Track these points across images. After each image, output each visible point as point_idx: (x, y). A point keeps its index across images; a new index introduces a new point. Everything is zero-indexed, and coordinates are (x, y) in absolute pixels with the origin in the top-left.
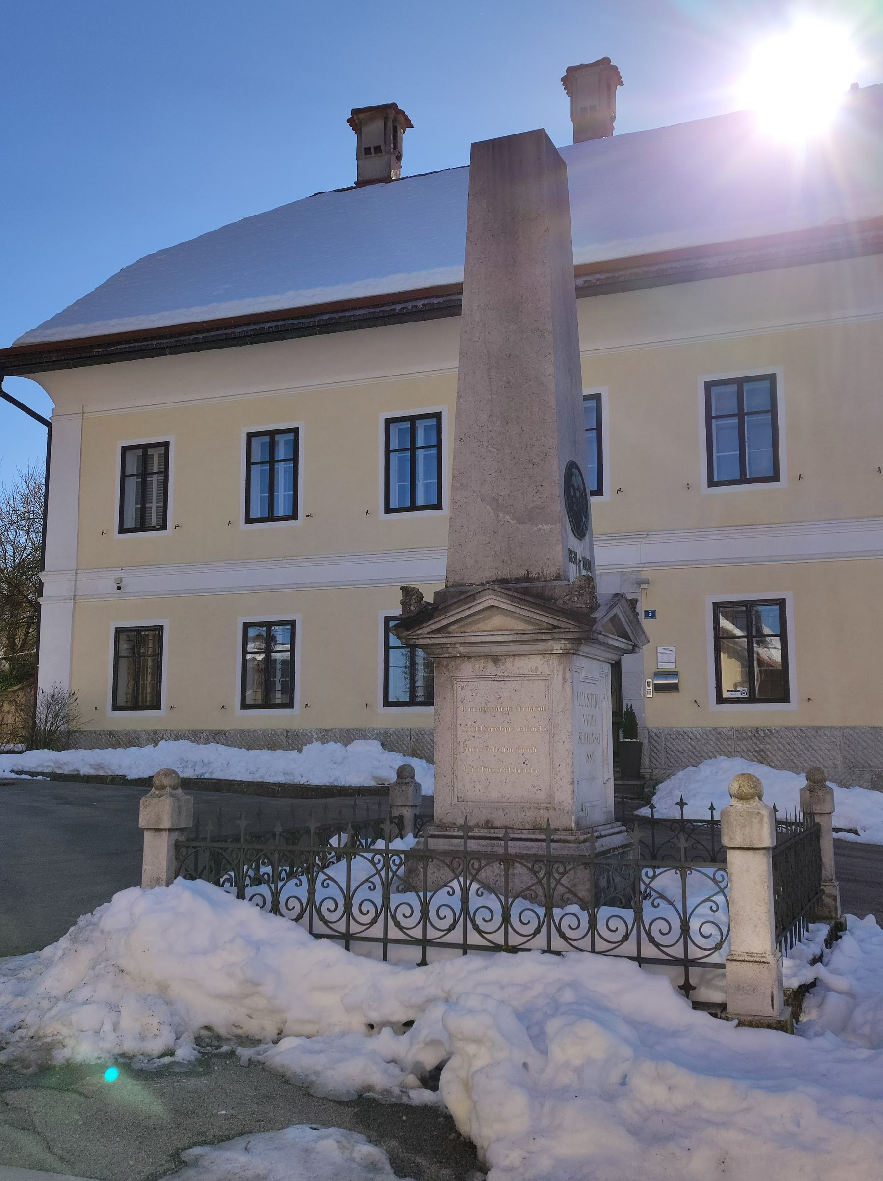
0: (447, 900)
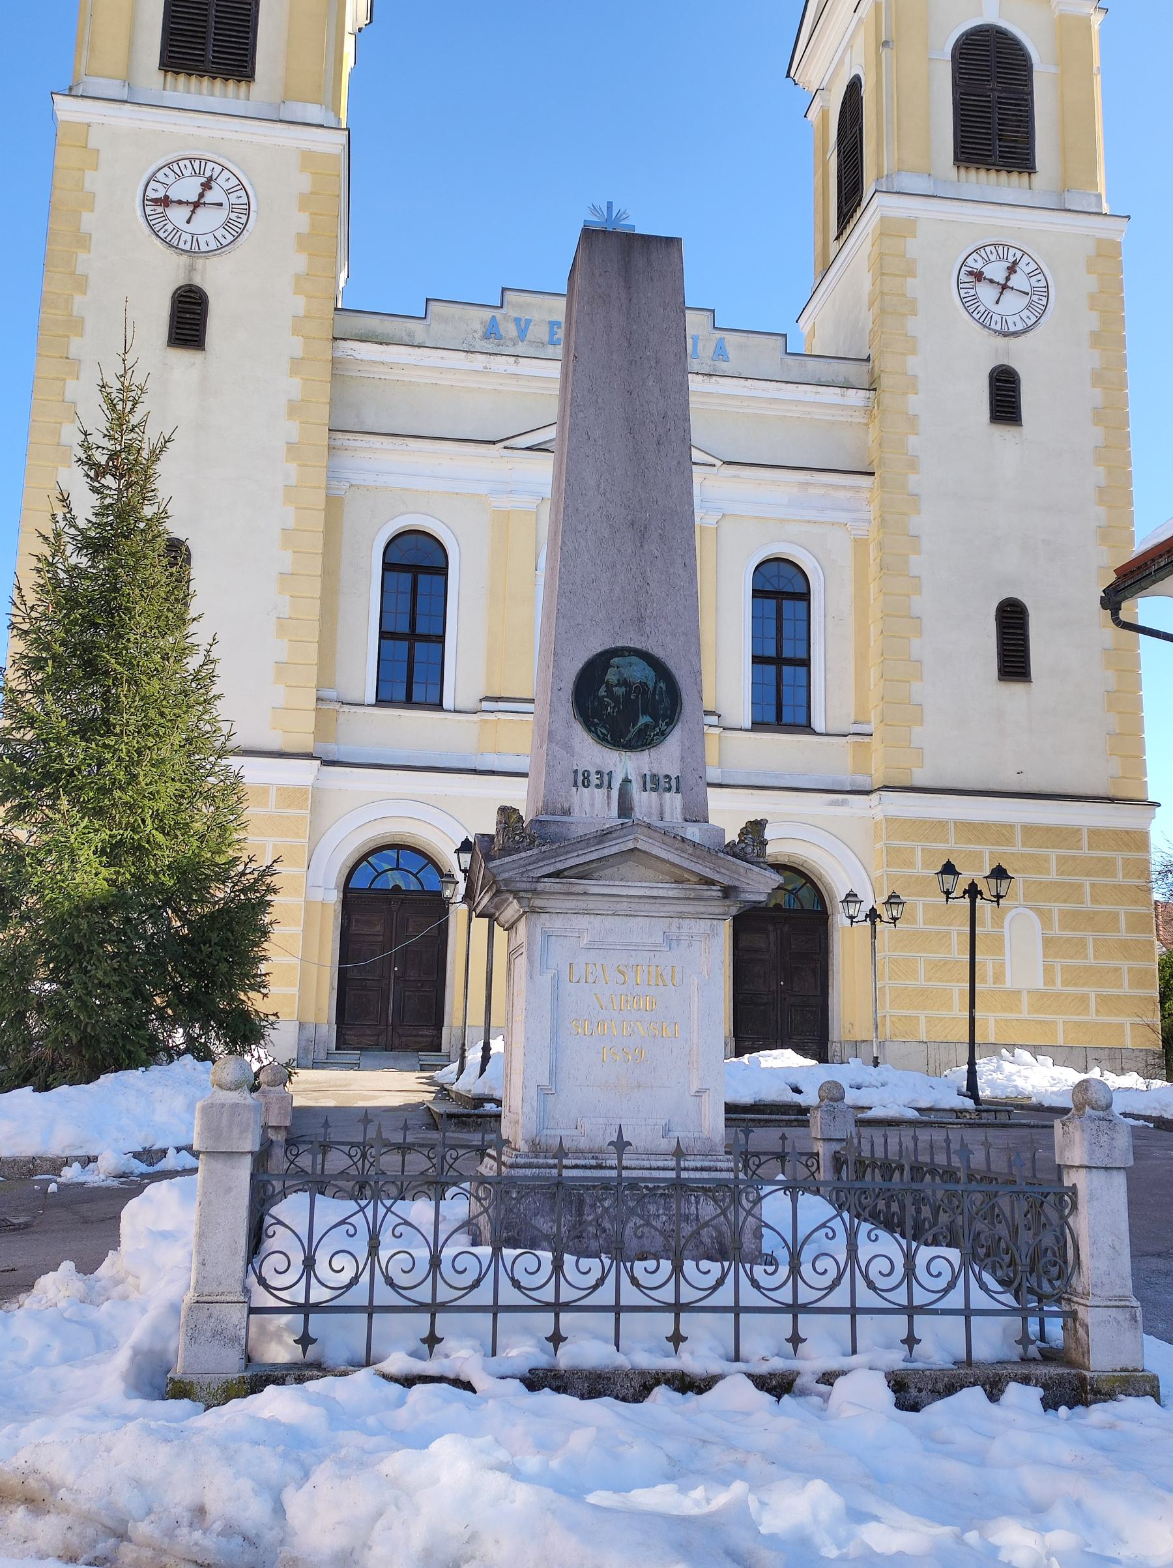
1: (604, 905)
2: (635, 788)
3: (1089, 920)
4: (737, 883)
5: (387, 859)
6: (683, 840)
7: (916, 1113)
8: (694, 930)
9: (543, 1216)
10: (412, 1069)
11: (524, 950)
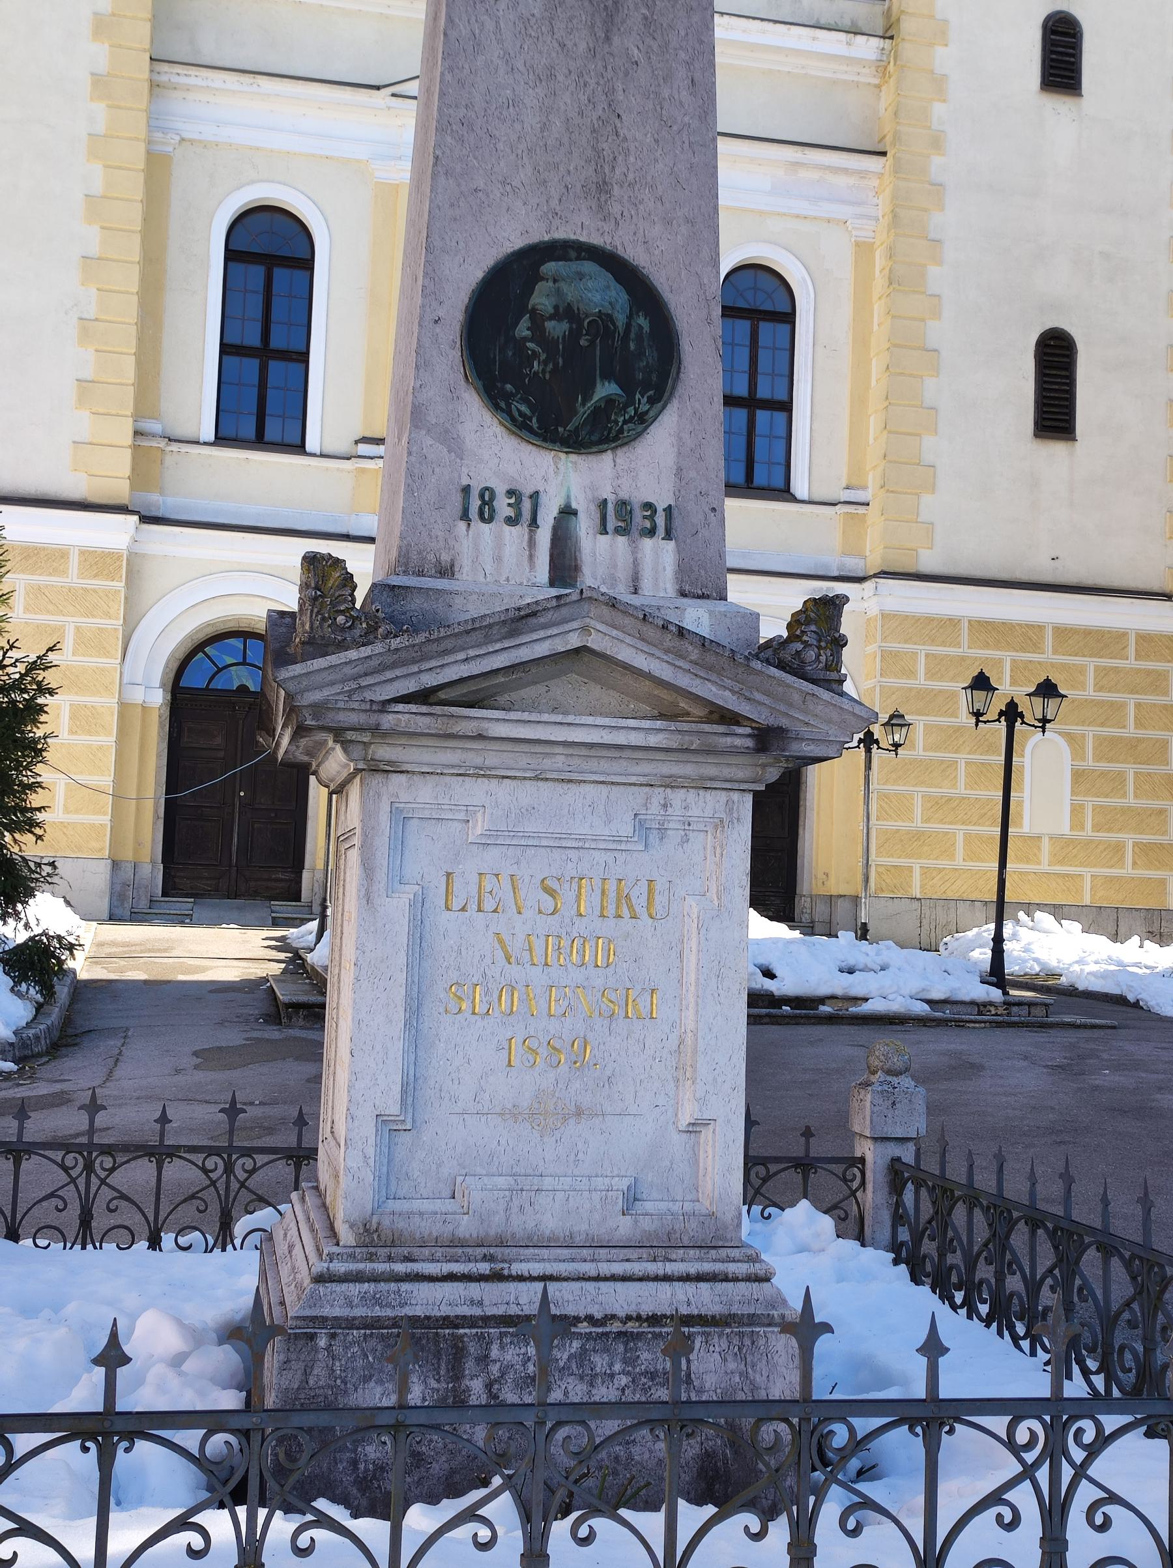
1: (521, 760)
2: (584, 526)
3: (1132, 749)
4: (784, 722)
5: (231, 651)
6: (681, 632)
7: (926, 1007)
8: (695, 811)
9: (380, 1382)
10: (261, 925)
11: (356, 840)
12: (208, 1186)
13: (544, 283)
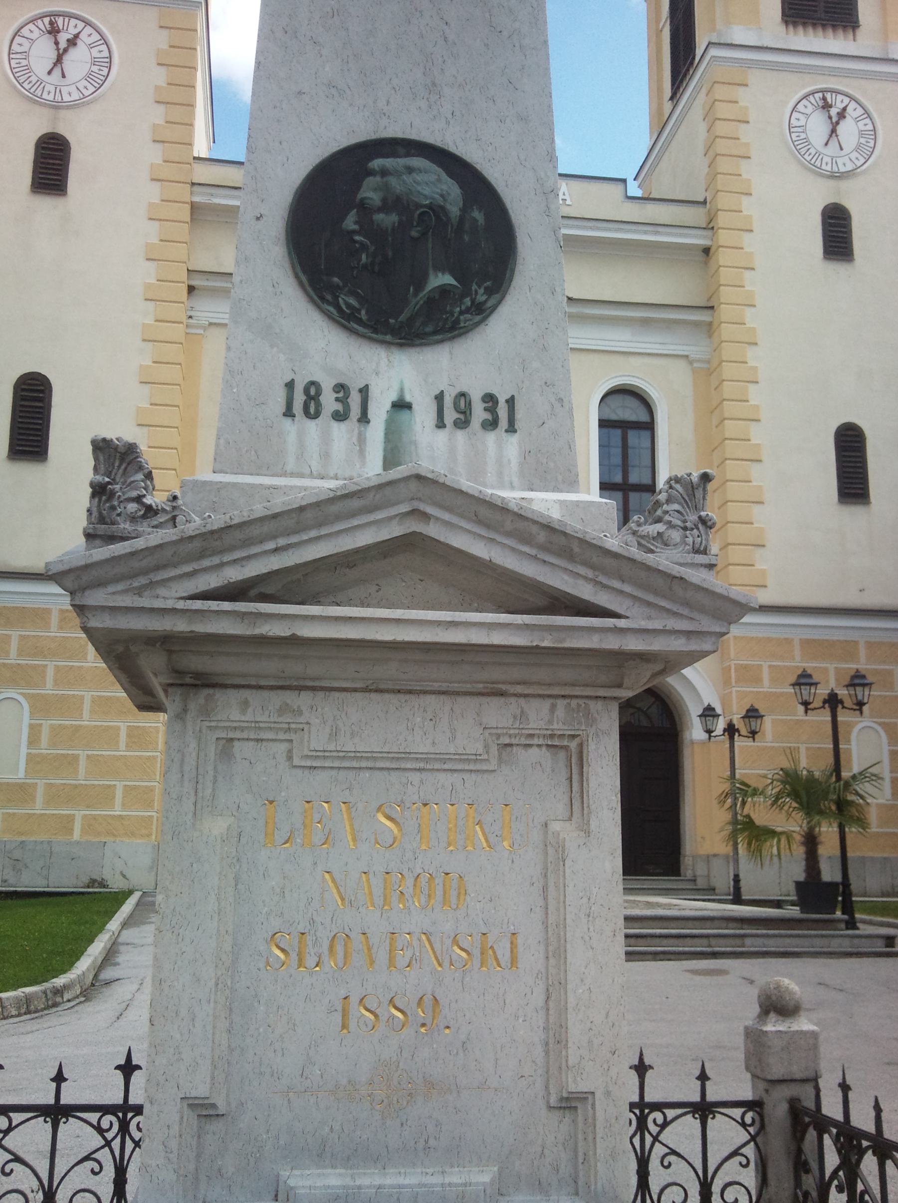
0: (91, 1182)
2: (423, 415)
12: (102, 1147)
13: (371, 178)
